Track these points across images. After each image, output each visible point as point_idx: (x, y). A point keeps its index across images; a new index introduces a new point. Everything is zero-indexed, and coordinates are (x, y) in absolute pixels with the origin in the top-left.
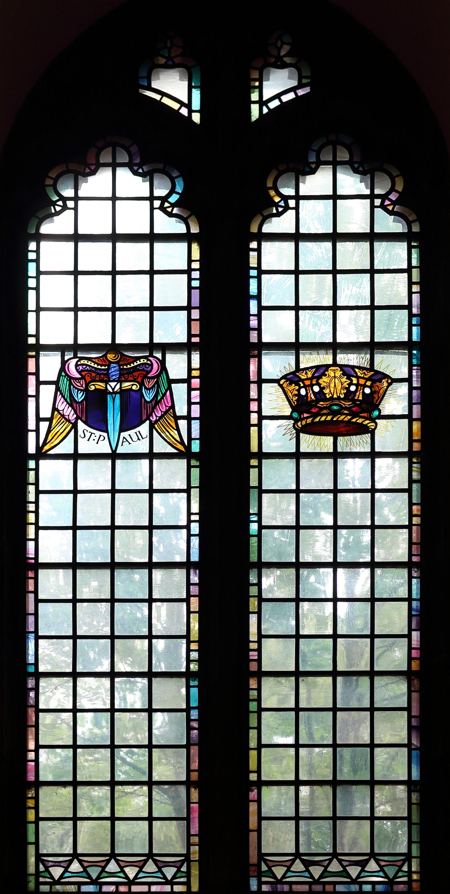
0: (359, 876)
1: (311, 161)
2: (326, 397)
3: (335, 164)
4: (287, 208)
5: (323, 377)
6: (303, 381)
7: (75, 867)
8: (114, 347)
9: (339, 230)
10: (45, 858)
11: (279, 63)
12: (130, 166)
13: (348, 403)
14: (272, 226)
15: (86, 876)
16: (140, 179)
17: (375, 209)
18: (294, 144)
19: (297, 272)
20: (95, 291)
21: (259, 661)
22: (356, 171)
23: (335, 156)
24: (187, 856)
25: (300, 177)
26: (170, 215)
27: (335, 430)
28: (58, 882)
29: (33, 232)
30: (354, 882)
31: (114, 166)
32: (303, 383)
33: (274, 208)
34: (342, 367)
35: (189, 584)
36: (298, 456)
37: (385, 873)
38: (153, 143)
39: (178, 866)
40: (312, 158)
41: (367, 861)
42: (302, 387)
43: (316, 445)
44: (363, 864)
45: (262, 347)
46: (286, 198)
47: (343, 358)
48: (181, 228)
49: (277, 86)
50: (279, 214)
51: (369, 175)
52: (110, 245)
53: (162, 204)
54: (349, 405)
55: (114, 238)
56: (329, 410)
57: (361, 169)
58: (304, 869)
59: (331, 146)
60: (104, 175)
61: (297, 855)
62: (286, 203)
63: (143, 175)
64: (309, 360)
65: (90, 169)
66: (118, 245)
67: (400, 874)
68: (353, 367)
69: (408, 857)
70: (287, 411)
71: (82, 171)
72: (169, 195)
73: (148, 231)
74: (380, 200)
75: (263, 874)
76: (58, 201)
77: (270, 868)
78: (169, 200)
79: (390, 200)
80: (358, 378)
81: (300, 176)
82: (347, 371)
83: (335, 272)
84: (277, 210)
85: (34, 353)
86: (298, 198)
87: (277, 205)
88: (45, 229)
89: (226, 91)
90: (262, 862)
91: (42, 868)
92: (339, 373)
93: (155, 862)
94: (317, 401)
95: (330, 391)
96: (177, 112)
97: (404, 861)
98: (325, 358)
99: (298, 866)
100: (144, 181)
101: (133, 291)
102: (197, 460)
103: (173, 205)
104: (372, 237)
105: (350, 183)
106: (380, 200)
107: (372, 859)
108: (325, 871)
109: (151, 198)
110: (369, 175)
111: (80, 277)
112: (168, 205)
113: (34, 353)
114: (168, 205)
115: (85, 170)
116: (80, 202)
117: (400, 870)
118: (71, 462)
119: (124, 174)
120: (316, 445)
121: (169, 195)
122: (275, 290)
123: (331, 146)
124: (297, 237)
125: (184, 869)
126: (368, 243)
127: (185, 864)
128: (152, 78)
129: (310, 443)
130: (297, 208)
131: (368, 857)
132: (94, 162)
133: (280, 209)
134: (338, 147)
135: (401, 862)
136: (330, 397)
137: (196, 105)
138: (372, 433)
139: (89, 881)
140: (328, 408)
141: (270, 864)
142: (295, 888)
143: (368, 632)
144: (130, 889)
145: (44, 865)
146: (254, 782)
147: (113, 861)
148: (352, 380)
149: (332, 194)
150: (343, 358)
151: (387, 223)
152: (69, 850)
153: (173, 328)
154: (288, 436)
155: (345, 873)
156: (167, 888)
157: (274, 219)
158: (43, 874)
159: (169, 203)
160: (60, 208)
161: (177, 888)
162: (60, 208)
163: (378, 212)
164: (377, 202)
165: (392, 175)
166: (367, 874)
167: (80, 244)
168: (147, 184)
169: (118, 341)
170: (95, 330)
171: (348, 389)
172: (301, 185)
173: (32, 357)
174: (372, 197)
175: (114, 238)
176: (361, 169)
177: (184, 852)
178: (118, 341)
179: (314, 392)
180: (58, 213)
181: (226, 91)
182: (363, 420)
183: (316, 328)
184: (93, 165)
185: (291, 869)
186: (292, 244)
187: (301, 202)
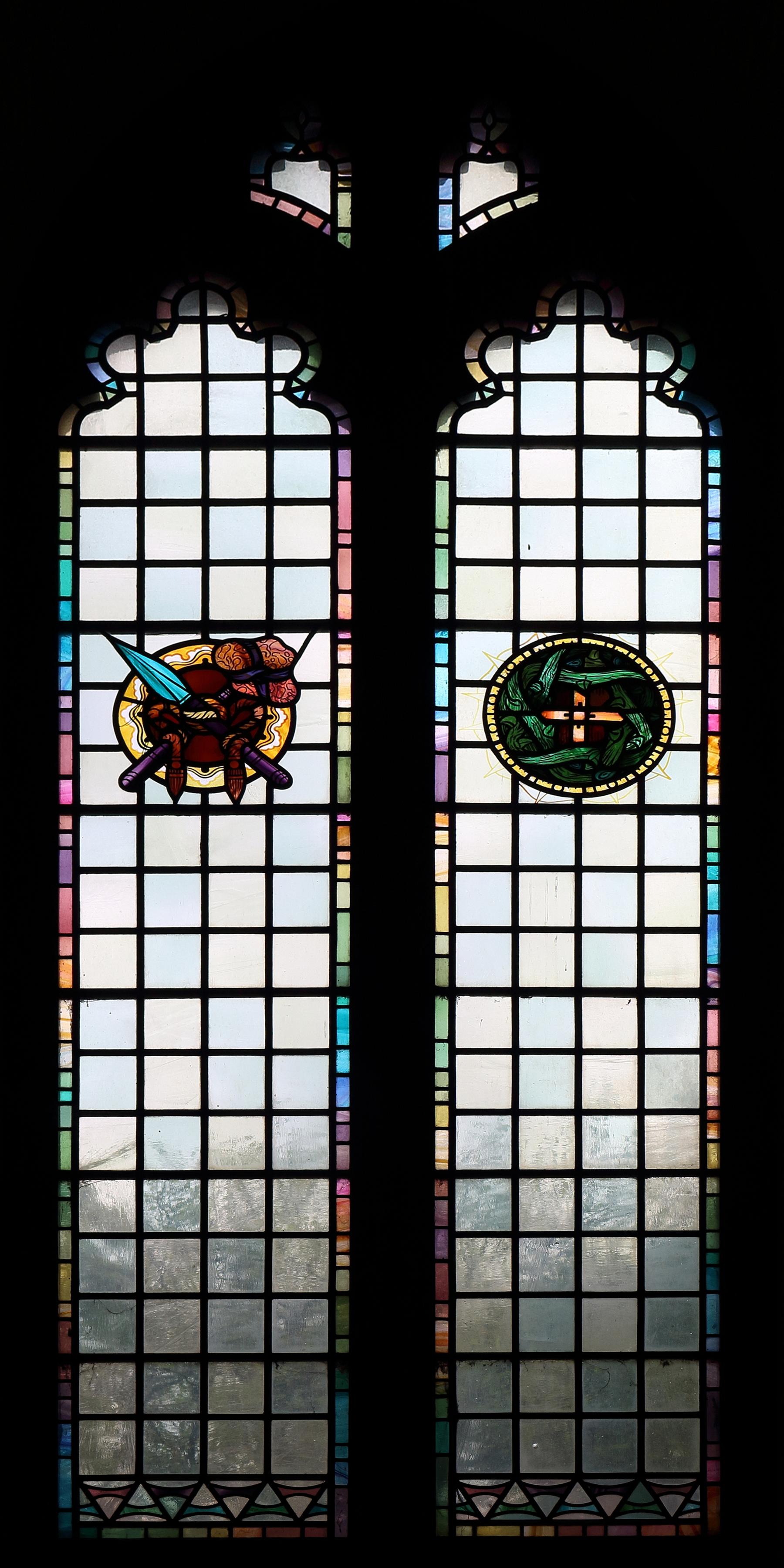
0: (554, 1512)
1: (541, 316)
7: (268, 1497)
8: (579, 626)
9: (213, 431)
10: (280, 1482)
11: (301, 153)
12: (605, 321)
14: (95, 424)
15: (533, 1510)
17: (275, 397)
23: (204, 311)
24: (328, 1480)
26: (670, 403)
28: (112, 1523)
30: (670, 1521)
33: (477, 394)
36: (515, 809)
37: (661, 1505)
38: (271, 282)
39: (625, 1491)
40: (164, 312)
41: (568, 1488)
46: (120, 378)
49: (484, 186)
50: (485, 403)
52: (198, 454)
53: (660, 386)
57: (248, 330)
58: (652, 1500)
59: (575, 291)
62: (499, 386)
63: (253, 337)
66: (278, 454)
71: (525, 330)
73: (198, 432)
74: (283, 382)
75: (325, 1510)
77: (469, 1497)
79: (672, 382)
81: (522, 341)
83: (579, 502)
84: (482, 395)
85: (445, 635)
87: (103, 388)
89: (395, 191)
97: (693, 1486)
105: (607, 350)
106: (283, 382)
107: (578, 1484)
109: (269, 376)
113: (445, 635)
115: (531, 329)
117: (687, 1501)
121: (671, 370)
122: (480, 532)
123: (575, 291)
125: (324, 1499)
126: (699, 452)
127: (698, 1491)
130: (516, 395)
131: (196, 1482)
132: (169, 317)
133: (110, 396)
135: (689, 1488)
137: (344, 219)
141: (94, 1493)
142: (272, 1533)
144: (606, 1531)
145: (89, 1496)
146: (442, 1355)
149: (135, 372)
152: (197, 1471)
153: (307, 595)
156: (172, 1533)
158: (86, 1510)
159: (299, 381)
160: (674, 392)
161: (686, 1530)
163: (651, 400)
164: (651, 385)
165: (302, 340)
166: (193, 1510)
169: (586, 617)
170: (548, 597)
173: (442, 641)
174: (642, 376)
175: (580, 442)
176: (248, 330)
177: (324, 1471)
178: (586, 617)
184: (166, 321)
185: (567, 1501)
186: (262, 454)
187: (147, 385)
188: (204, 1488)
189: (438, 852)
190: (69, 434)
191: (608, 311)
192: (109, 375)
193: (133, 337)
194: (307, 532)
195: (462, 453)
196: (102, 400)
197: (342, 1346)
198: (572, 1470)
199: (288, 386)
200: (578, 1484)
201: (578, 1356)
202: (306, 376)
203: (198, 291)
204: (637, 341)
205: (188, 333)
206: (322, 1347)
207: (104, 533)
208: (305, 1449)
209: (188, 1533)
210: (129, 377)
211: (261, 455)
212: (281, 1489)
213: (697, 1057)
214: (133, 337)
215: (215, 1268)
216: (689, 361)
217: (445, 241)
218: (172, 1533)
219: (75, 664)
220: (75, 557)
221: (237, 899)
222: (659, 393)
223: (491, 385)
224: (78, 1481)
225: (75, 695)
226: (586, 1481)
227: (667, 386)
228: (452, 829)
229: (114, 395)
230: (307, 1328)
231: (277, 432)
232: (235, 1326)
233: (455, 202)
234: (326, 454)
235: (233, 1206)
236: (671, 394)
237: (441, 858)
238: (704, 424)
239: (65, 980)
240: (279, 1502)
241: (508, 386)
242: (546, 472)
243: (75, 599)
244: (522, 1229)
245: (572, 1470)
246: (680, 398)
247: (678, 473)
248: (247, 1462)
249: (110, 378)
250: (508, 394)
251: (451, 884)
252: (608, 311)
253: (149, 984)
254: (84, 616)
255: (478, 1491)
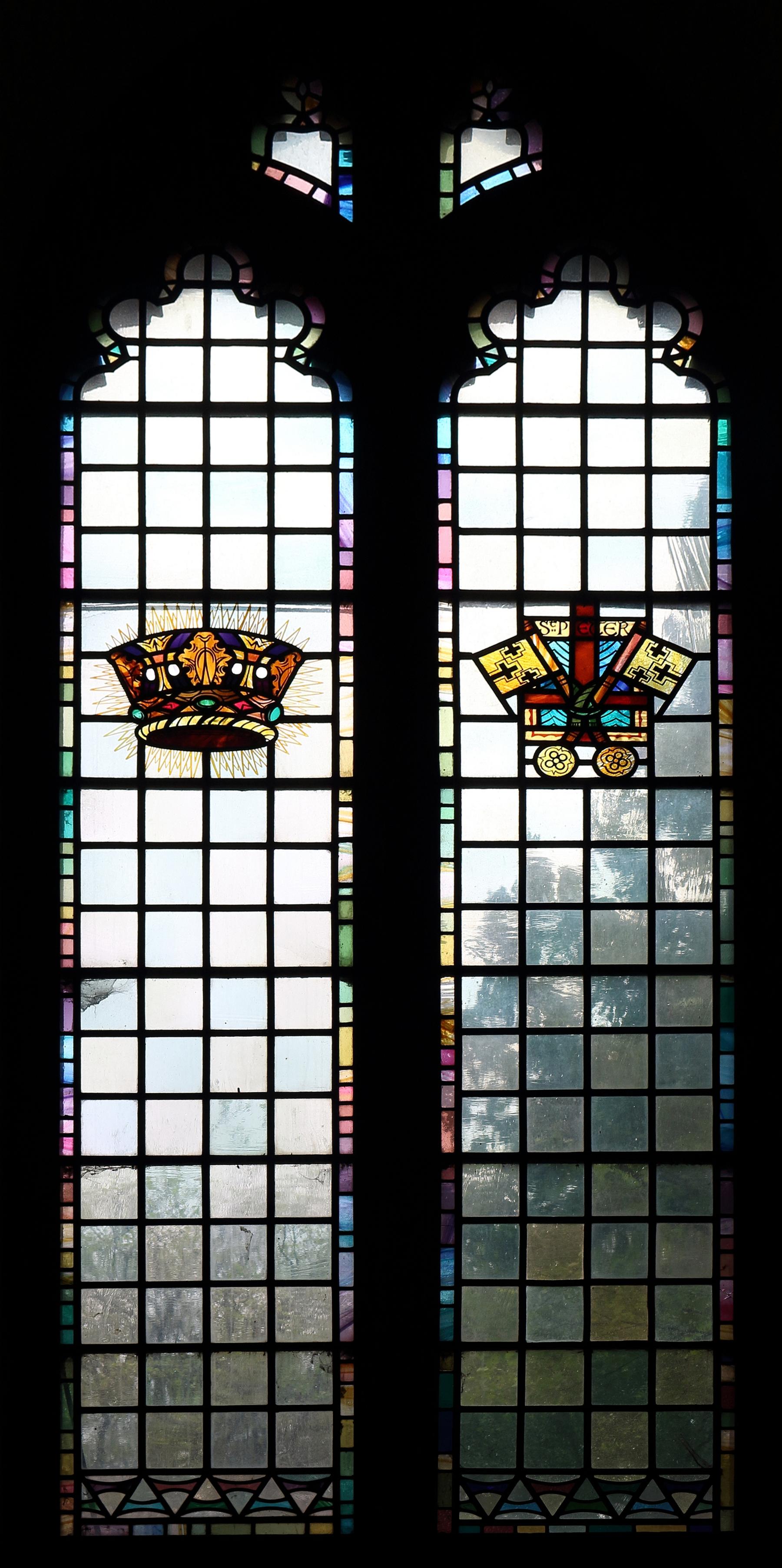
2: (191, 684)
3: (585, 288)
4: (502, 359)
5: (185, 650)
6: (150, 655)
7: (143, 1492)
9: (214, 398)
12: (234, 286)
13: (227, 694)
16: (252, 308)
18: (520, 252)
19: (649, 470)
20: (552, 501)
21: (77, 1135)
22: (621, 301)
25: (526, 308)
26: (679, 371)
27: (204, 741)
29: (69, 397)
31: (208, 286)
32: (152, 660)
34: (217, 632)
35: (336, 1005)
36: (141, 784)
38: (271, 251)
42: (150, 667)
43: (172, 763)
44: (127, 1488)
45: (81, 597)
46: (500, 344)
47: (224, 617)
48: (324, 395)
49: (485, 154)
50: (488, 371)
51: (266, 306)
52: (264, 421)
53: (289, 353)
54: (230, 697)
55: (585, 411)
56: (196, 707)
60: (568, 302)
61: (142, 1472)
64: (163, 619)
65: (544, 293)
66: (656, 423)
67: (701, 1507)
68: (236, 633)
69: (334, 1474)
70: (123, 706)
72: (303, 336)
76: (112, 346)
77: (471, 1495)
78: (302, 344)
80: (246, 651)
82: (229, 640)
83: (520, 470)
84: (484, 362)
86: (143, 342)
88: (467, 395)
89: (394, 157)
90: (331, 1485)
91: (464, 1497)
92: (213, 642)
93: (151, 1484)
94: (254, 692)
95: (197, 675)
96: (308, 198)
98: (187, 617)
99: (143, 1492)
100: (258, 315)
101: (617, 502)
102: (727, 790)
103: (308, 352)
104: (271, 410)
107: (207, 1480)
108: (190, 1499)
110: (266, 306)
111: (200, 475)
112: (301, 352)
114: (301, 352)
116: (149, 349)
117: (319, 1498)
118: (198, 794)
119: (225, 302)
120: (172, 763)
121: (303, 336)
122: (482, 500)
124: (142, 409)
128: (462, 139)
129: (164, 762)
130: (519, 360)
134: (148, 303)
136: (198, 684)
138: (271, 746)
139: (544, 1518)
140: (194, 702)
143: (580, 1086)
145: (90, 1490)
147: (143, 1482)
148: (234, 656)
149: (515, 338)
150: (224, 617)
151: (672, 388)
152: (133, 1464)
154: (125, 752)
155: (224, 1503)
156: (298, 1529)
157: (479, 379)
158: (87, 1506)
159: (302, 348)
160: (116, 358)
162: (116, 358)
163: (658, 368)
167: (591, 422)
168: (265, 320)
169: (592, 587)
171: (228, 670)
172: (526, 320)
174: (271, 342)
177: (329, 1464)
178: (592, 587)
179: (169, 677)
180: (112, 367)
181: (394, 157)
182: (155, 724)
183: (174, 564)
184: (172, 282)
185: (261, 1496)
186: (134, 421)
187: (149, 349)
188: (272, 1481)
189: (443, 827)
190: (448, 401)
191: (613, 277)
192: (113, 339)
193: (136, 302)
194: (308, 500)
195: (463, 422)
196: (104, 363)
197: (727, 1333)
198: (265, 1465)
199: (667, 354)
200: (207, 1480)
201: (587, 1347)
202: (308, 343)
203: (581, 257)
204: (644, 308)
205: (569, 300)
206: (327, 1337)
207: (104, 499)
208: (309, 1442)
209: (262, 1529)
210: (510, 343)
211: (639, 424)
212: (156, 1485)
213: (710, 1036)
214: (136, 302)
215: (663, 1254)
216: (695, 327)
217: (446, 206)
218: (243, 1530)
219: (77, 634)
220: (453, 523)
221: (238, 877)
222: (289, 359)
223: (494, 351)
224: (81, 1474)
225: (76, 666)
226: (280, 1476)
227: (298, 352)
228: (457, 805)
229: (116, 358)
230: (310, 1317)
231: (213, 399)
232: (241, 1315)
233: (456, 167)
234: (327, 422)
235: (236, 1190)
236: (302, 361)
237: (447, 832)
238: (712, 394)
239: (447, 958)
240: (219, 1497)
241: (511, 352)
242: (549, 441)
243: (77, 565)
244: (148, 1216)
245: (265, 1465)
246: (687, 366)
247: (688, 441)
248: (187, 1457)
249: (490, 343)
250: (134, 358)
251: (457, 860)
252: (613, 277)
253: (278, 963)
254: (86, 585)
255: (233, 1486)
